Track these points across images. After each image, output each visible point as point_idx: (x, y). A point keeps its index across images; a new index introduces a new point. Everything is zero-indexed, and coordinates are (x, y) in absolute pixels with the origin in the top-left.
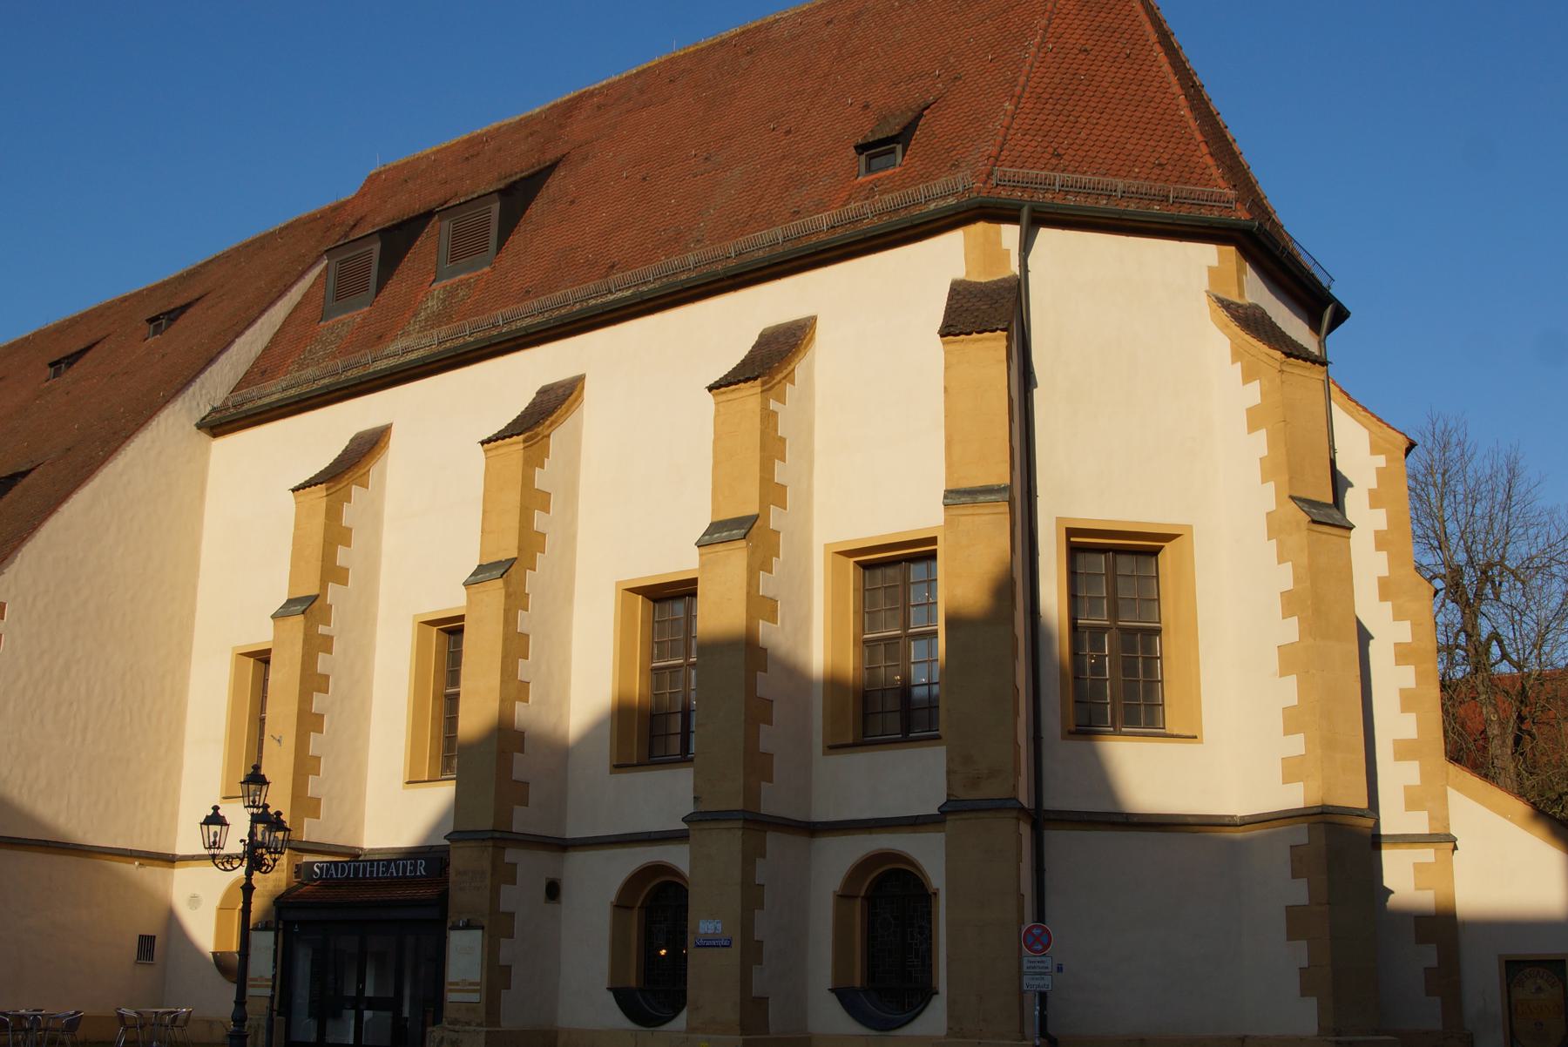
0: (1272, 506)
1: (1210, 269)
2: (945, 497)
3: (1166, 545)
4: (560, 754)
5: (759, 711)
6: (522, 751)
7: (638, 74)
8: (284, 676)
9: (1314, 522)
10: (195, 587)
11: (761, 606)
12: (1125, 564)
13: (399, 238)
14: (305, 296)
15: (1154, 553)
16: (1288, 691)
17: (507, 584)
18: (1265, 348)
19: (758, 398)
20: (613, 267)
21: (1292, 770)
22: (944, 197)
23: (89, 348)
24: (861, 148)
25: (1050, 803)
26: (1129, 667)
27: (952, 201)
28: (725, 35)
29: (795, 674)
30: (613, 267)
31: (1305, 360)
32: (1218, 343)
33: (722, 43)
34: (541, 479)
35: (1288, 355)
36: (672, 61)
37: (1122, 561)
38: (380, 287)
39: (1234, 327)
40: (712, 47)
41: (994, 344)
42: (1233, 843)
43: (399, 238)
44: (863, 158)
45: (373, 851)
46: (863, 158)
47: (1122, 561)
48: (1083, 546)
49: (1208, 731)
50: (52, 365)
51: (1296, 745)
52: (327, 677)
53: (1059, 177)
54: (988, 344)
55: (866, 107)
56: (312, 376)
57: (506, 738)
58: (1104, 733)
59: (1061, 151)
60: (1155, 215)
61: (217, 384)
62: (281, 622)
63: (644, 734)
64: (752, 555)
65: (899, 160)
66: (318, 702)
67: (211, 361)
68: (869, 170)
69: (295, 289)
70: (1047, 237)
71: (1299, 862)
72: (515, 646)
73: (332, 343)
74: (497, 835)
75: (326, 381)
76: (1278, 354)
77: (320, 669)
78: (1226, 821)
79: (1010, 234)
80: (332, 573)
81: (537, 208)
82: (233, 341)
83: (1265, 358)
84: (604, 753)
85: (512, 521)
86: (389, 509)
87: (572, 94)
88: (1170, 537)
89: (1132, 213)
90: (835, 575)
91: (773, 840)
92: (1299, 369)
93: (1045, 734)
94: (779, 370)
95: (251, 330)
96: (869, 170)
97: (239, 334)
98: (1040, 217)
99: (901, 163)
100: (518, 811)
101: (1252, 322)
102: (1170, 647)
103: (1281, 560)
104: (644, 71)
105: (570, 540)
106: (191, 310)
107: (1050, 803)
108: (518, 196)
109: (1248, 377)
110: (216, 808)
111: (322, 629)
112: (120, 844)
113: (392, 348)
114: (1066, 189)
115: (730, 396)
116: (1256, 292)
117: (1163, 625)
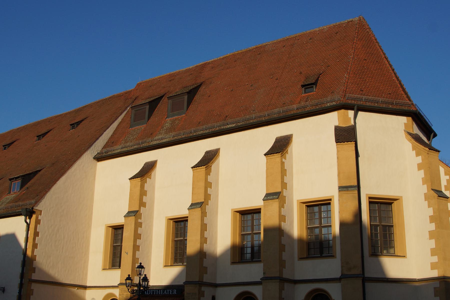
0: (426, 192)
1: (405, 123)
2: (339, 189)
3: (395, 202)
4: (215, 259)
5: (282, 248)
6: (206, 258)
7: (223, 58)
8: (128, 234)
9: (439, 196)
10: (92, 206)
11: (282, 218)
12: (383, 207)
13: (154, 104)
14: (123, 119)
15: (391, 204)
16: (432, 244)
17: (202, 209)
18: (423, 147)
19: (280, 158)
20: (226, 117)
21: (433, 266)
22: (332, 102)
23: (49, 132)
24: (303, 86)
25: (367, 275)
26: (385, 236)
27: (334, 103)
28: (250, 48)
29: (290, 237)
30: (226, 117)
31: (434, 150)
32: (408, 145)
33: (250, 51)
34: (210, 179)
35: (430, 149)
36: (234, 55)
37: (383, 206)
38: (148, 120)
39: (413, 141)
40: (247, 52)
41: (351, 145)
42: (416, 287)
43: (154, 104)
44: (303, 89)
45: (153, 286)
46: (303, 89)
47: (383, 206)
48: (374, 202)
49: (408, 255)
50: (37, 137)
51: (435, 259)
52: (141, 235)
53: (364, 97)
54: (349, 145)
55: (301, 73)
56: (131, 145)
57: (202, 255)
58: (380, 255)
59: (363, 89)
60: (390, 108)
61: (98, 146)
62: (127, 218)
63: (239, 254)
64: (280, 203)
65: (314, 90)
66: (138, 242)
67: (97, 139)
68: (305, 92)
69: (120, 118)
70: (361, 114)
71: (437, 292)
72: (204, 227)
73: (135, 135)
74: (200, 283)
75: (136, 146)
76: (427, 149)
77: (139, 232)
78: (414, 280)
79: (351, 113)
80: (142, 204)
81: (197, 97)
82: (103, 133)
83: (423, 150)
84: (228, 259)
85: (202, 191)
86: (157, 185)
87: (202, 63)
88: (396, 200)
89: (385, 108)
90: (300, 209)
91: (286, 285)
92: (432, 153)
93: (365, 255)
94: (285, 150)
95: (108, 130)
96: (305, 92)
97: (105, 131)
98: (359, 108)
99: (315, 91)
100: (205, 275)
101: (416, 138)
102: (396, 231)
103: (429, 207)
104: (225, 57)
105: (217, 196)
106: (83, 122)
107: (367, 275)
108: (192, 93)
109: (417, 155)
110: (129, 275)
111: (139, 221)
112: (72, 283)
113: (157, 138)
114: (366, 101)
115: (271, 157)
116: (416, 131)
117: (394, 224)
